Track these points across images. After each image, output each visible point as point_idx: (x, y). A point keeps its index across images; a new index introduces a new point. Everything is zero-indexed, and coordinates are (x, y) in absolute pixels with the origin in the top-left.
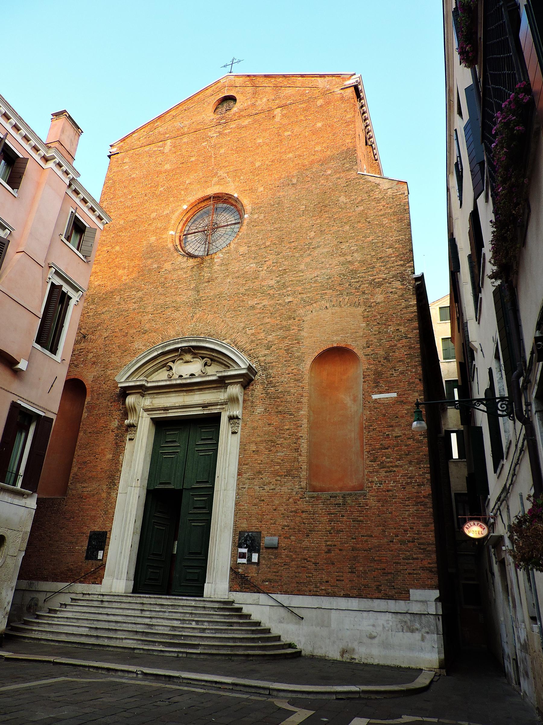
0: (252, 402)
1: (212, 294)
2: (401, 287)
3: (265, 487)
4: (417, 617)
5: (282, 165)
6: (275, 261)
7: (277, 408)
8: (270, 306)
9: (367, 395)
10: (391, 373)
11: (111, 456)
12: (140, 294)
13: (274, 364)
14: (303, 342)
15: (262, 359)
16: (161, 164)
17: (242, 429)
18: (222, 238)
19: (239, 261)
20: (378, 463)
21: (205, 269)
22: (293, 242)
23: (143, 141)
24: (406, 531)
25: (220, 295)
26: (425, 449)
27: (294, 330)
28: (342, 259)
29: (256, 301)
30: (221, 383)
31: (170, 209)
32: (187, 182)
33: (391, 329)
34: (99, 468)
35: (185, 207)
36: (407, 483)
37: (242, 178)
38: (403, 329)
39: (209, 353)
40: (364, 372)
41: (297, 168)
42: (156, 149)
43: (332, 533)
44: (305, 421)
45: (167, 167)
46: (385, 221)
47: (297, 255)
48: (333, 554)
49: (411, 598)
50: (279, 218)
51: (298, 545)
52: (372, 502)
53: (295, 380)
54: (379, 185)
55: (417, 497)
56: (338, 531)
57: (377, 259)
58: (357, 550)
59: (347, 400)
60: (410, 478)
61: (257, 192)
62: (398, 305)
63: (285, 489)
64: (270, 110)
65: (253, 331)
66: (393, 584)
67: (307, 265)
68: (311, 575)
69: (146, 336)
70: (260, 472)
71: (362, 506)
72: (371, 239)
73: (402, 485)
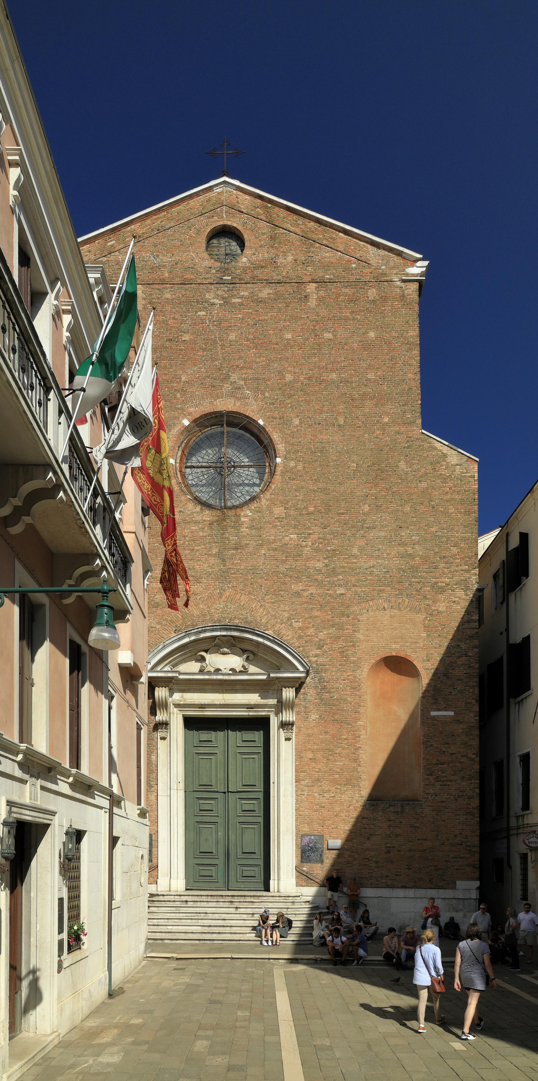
0: (306, 708)
3: (325, 795)
7: (333, 716)
14: (358, 646)
17: (296, 735)
21: (230, 530)
24: (456, 836)
29: (300, 587)
32: (183, 379)
35: (186, 422)
36: (459, 796)
37: (267, 394)
38: (463, 646)
47: (349, 533)
49: (457, 888)
50: (324, 474)
53: (352, 688)
54: (445, 456)
57: (440, 558)
65: (300, 624)
70: (318, 780)
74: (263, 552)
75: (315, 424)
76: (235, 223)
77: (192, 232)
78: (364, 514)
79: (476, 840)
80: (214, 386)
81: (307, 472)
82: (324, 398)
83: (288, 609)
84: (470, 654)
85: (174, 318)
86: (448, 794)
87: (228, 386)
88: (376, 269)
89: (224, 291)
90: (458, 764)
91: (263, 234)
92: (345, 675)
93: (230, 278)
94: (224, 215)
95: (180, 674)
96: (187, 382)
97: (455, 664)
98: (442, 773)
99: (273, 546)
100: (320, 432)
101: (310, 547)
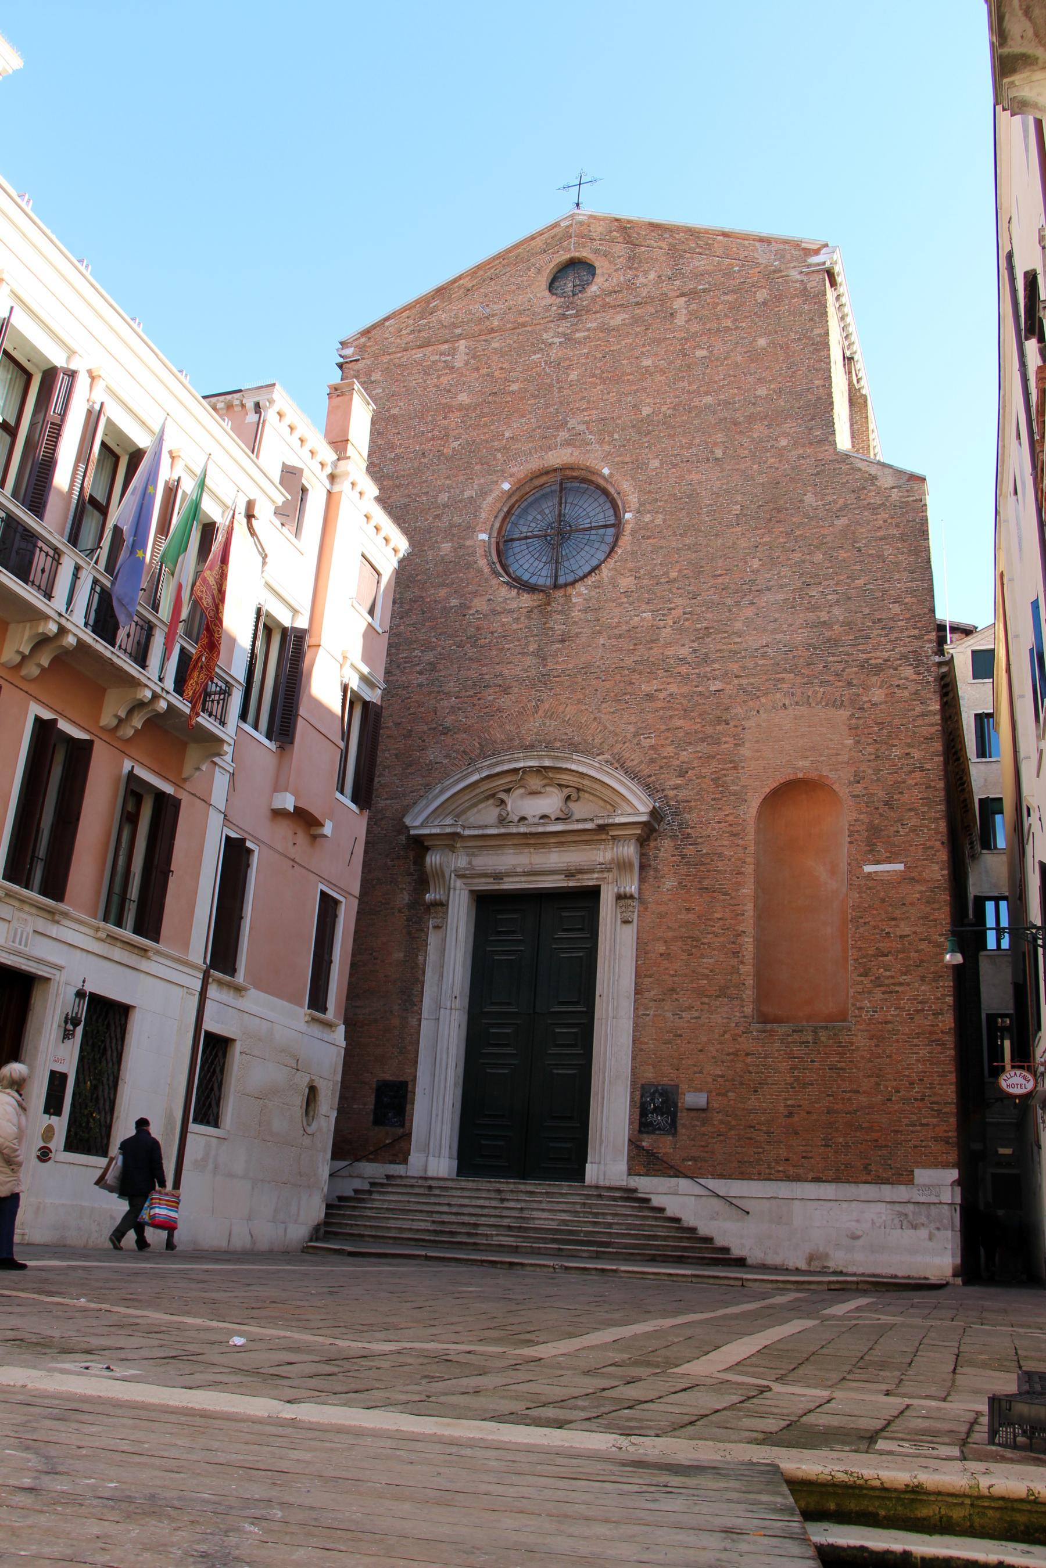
1: (570, 666)
2: (914, 677)
3: (684, 1015)
4: (923, 1207)
6: (687, 610)
7: (699, 882)
9: (854, 866)
10: (895, 829)
11: (402, 955)
12: (429, 656)
13: (693, 804)
15: (671, 793)
16: (449, 391)
19: (620, 605)
22: (721, 575)
28: (811, 616)
29: (655, 685)
31: (476, 487)
32: (507, 435)
33: (897, 752)
35: (506, 486)
36: (917, 1011)
37: (616, 436)
38: (916, 754)
39: (575, 779)
42: (437, 358)
44: (750, 906)
45: (463, 398)
48: (796, 1118)
49: (916, 1182)
51: (740, 1105)
52: (861, 1040)
54: (875, 478)
55: (931, 1033)
56: (805, 1085)
59: (822, 872)
62: (909, 710)
67: (748, 622)
68: (761, 1150)
69: (449, 740)
70: (673, 990)
72: (860, 582)
76: (584, 253)
79: (949, 1093)
84: (927, 766)
85: (501, 368)
86: (896, 1009)
88: (766, 267)
90: (913, 954)
91: (619, 257)
92: (722, 814)
96: (512, 438)
98: (886, 970)
99: (616, 631)
100: (688, 471)
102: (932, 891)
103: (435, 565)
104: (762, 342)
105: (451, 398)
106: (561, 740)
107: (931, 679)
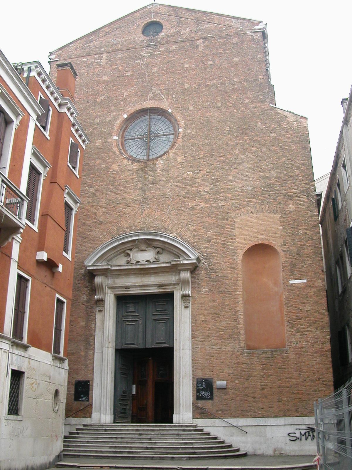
0: (199, 284)
3: (214, 347)
5: (208, 90)
7: (218, 289)
8: (207, 207)
10: (302, 265)
11: (84, 323)
12: (92, 190)
17: (192, 304)
18: (160, 146)
20: (294, 329)
23: (79, 52)
24: (314, 373)
25: (164, 196)
26: (327, 319)
27: (228, 229)
30: (175, 269)
32: (125, 94)
33: (301, 232)
34: (75, 333)
35: (125, 116)
36: (315, 342)
37: (174, 96)
38: (309, 232)
39: (161, 244)
40: (283, 264)
41: (220, 93)
43: (264, 377)
45: (105, 78)
46: (293, 147)
47: (226, 167)
50: (209, 135)
52: (292, 356)
54: (286, 117)
57: (288, 177)
58: (282, 387)
60: (316, 339)
61: (188, 110)
63: (228, 348)
64: (194, 40)
66: (306, 407)
68: (251, 405)
69: (103, 227)
70: (209, 336)
71: (285, 359)
72: (283, 160)
73: (311, 344)
74: (170, 184)
75: (203, 108)
76: (165, 104)
77: (135, 27)
78: (236, 155)
80: (143, 96)
81: (199, 135)
82: (209, 94)
83: (186, 218)
87: (151, 94)
89: (151, 49)
90: (312, 318)
93: (154, 43)
94: (152, 17)
95: (112, 266)
97: (304, 246)
98: (301, 325)
101: (201, 178)
102: (319, 291)
103: (94, 150)
104: (236, 59)
105: (100, 78)
106: (153, 227)
107: (314, 201)
